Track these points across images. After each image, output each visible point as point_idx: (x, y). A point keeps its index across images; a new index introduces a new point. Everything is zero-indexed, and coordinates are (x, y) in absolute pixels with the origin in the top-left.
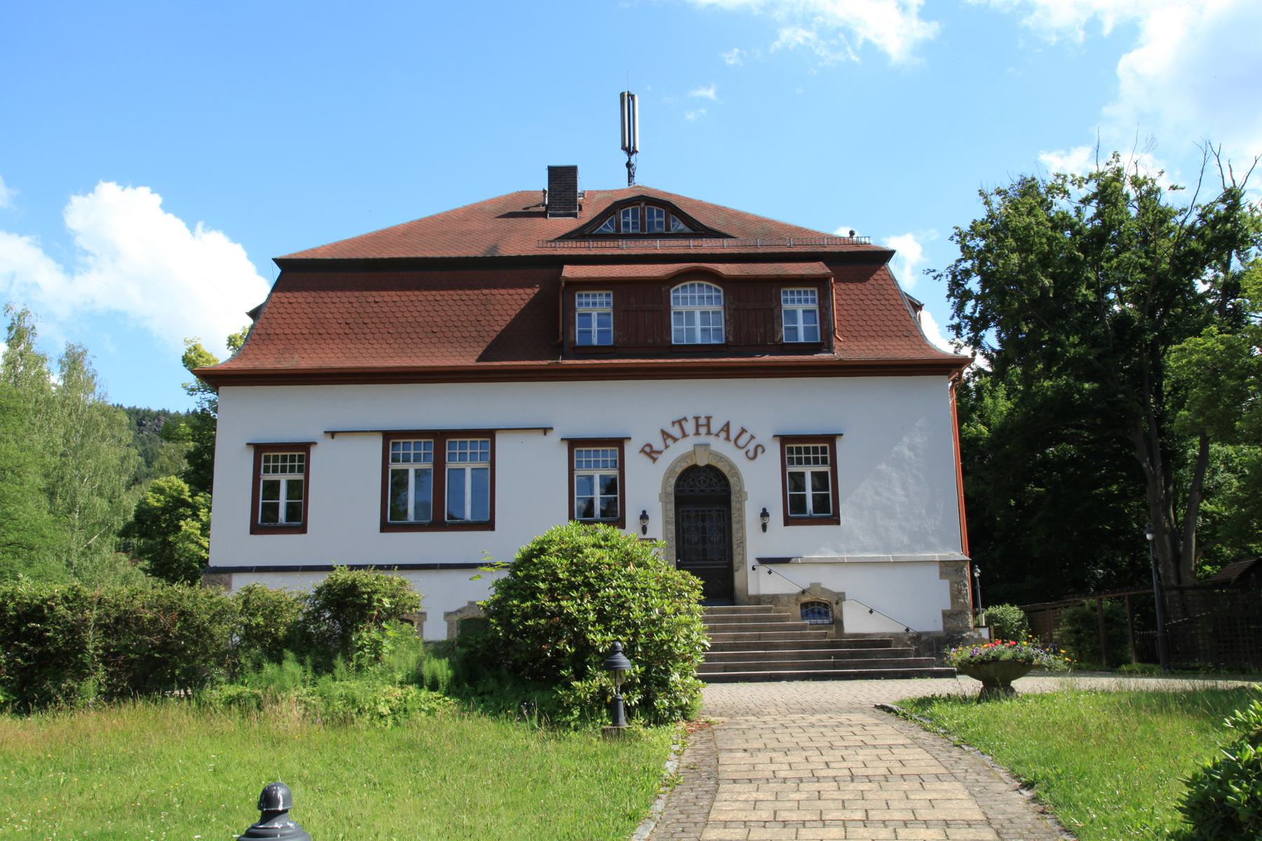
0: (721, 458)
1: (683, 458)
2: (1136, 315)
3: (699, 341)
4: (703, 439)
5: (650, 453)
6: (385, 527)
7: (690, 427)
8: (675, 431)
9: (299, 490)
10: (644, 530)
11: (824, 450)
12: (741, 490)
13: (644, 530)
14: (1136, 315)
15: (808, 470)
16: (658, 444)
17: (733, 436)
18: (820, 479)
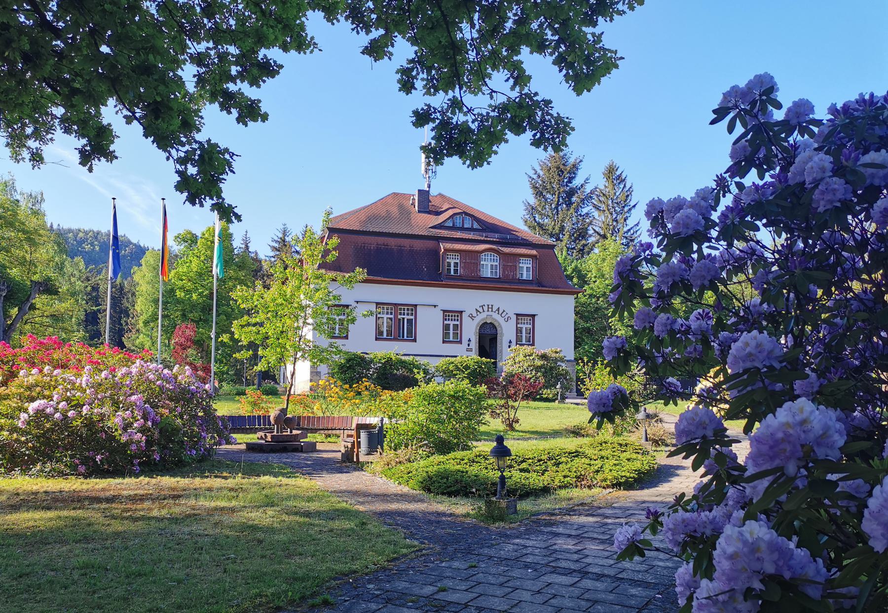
0: (496, 320)
1: (482, 320)
2: (881, 347)
3: (489, 276)
4: (490, 313)
5: (472, 317)
6: (377, 339)
7: (486, 308)
8: (480, 310)
9: (532, 331)
10: (469, 345)
11: (458, 316)
12: (502, 333)
13: (469, 345)
14: (881, 347)
15: (452, 323)
16: (474, 314)
17: (481, 311)
18: (456, 326)
